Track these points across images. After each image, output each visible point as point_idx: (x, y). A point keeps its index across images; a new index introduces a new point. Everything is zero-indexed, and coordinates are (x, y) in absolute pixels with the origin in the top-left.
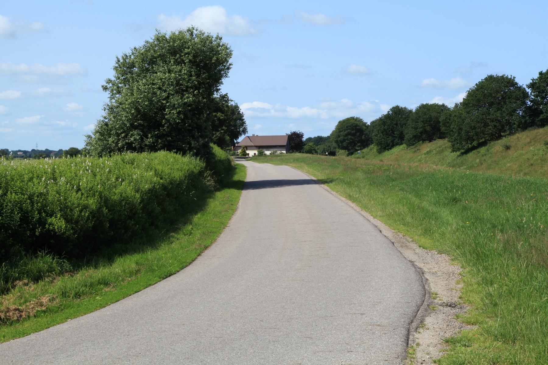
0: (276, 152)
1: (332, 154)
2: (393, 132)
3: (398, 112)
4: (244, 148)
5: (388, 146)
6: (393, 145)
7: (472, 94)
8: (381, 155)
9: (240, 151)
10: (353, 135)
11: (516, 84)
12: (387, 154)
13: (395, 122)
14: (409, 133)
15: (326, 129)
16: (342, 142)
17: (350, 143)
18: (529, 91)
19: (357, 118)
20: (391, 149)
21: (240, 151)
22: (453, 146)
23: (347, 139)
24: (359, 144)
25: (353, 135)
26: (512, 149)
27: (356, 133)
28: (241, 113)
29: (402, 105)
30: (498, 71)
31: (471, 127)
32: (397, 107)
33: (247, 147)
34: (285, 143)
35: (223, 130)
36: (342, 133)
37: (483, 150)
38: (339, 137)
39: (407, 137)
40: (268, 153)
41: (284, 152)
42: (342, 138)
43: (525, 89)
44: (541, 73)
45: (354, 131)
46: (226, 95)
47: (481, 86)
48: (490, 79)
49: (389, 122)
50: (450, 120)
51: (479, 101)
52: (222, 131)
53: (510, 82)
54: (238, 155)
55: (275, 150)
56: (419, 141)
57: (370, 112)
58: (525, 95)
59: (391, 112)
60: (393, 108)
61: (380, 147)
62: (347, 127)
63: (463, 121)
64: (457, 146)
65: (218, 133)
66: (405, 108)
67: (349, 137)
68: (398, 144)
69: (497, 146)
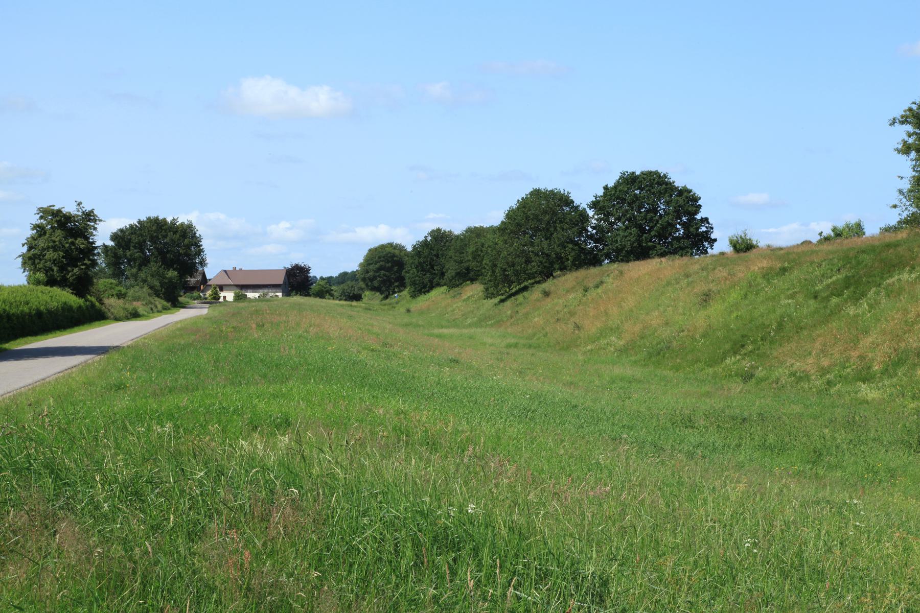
0: (267, 294)
1: (358, 298)
2: (432, 267)
3: (439, 238)
4: (215, 288)
5: (424, 287)
6: (432, 288)
7: (511, 215)
8: (414, 301)
9: (209, 293)
10: (389, 269)
11: (572, 202)
12: (422, 298)
13: (434, 253)
14: (451, 269)
15: (352, 263)
16: (372, 280)
17: (383, 282)
18: (591, 213)
19: (397, 245)
20: (428, 292)
21: (209, 293)
22: (487, 289)
23: (379, 276)
24: (396, 284)
25: (389, 269)
26: (552, 296)
27: (393, 266)
28: (197, 235)
29: (445, 227)
30: (547, 184)
31: (508, 263)
32: (439, 230)
33: (221, 288)
34: (280, 281)
35: (85, 264)
36: (371, 267)
37: (520, 297)
38: (368, 272)
39: (448, 275)
40: (251, 295)
41: (280, 295)
42: (371, 273)
43: (584, 209)
44: (606, 188)
45: (390, 264)
46: (92, 211)
47: (524, 204)
48: (536, 193)
49: (426, 251)
50: (482, 251)
51: (519, 225)
52: (83, 267)
53: (565, 200)
54: (206, 299)
55: (265, 291)
56: (464, 281)
57: (408, 237)
58: (583, 216)
59: (429, 238)
60: (433, 231)
61: (413, 289)
62: (379, 257)
63: (499, 253)
64: (491, 290)
65: (76, 270)
66: (450, 232)
67: (383, 272)
68: (439, 285)
69: (535, 294)
